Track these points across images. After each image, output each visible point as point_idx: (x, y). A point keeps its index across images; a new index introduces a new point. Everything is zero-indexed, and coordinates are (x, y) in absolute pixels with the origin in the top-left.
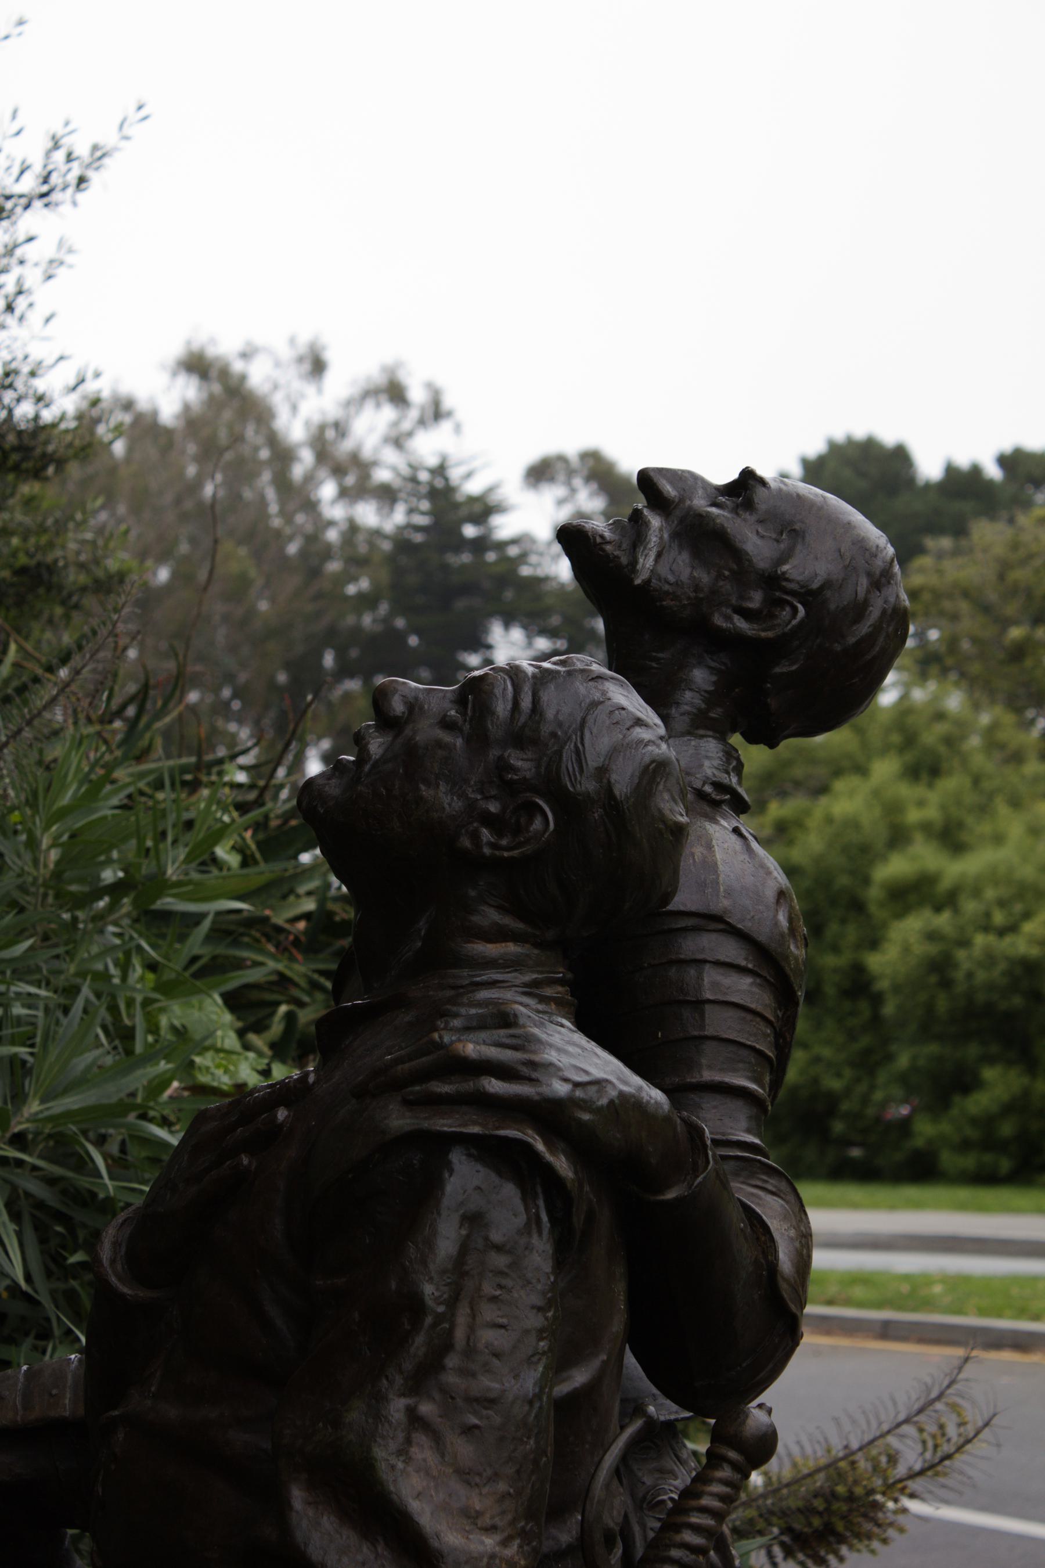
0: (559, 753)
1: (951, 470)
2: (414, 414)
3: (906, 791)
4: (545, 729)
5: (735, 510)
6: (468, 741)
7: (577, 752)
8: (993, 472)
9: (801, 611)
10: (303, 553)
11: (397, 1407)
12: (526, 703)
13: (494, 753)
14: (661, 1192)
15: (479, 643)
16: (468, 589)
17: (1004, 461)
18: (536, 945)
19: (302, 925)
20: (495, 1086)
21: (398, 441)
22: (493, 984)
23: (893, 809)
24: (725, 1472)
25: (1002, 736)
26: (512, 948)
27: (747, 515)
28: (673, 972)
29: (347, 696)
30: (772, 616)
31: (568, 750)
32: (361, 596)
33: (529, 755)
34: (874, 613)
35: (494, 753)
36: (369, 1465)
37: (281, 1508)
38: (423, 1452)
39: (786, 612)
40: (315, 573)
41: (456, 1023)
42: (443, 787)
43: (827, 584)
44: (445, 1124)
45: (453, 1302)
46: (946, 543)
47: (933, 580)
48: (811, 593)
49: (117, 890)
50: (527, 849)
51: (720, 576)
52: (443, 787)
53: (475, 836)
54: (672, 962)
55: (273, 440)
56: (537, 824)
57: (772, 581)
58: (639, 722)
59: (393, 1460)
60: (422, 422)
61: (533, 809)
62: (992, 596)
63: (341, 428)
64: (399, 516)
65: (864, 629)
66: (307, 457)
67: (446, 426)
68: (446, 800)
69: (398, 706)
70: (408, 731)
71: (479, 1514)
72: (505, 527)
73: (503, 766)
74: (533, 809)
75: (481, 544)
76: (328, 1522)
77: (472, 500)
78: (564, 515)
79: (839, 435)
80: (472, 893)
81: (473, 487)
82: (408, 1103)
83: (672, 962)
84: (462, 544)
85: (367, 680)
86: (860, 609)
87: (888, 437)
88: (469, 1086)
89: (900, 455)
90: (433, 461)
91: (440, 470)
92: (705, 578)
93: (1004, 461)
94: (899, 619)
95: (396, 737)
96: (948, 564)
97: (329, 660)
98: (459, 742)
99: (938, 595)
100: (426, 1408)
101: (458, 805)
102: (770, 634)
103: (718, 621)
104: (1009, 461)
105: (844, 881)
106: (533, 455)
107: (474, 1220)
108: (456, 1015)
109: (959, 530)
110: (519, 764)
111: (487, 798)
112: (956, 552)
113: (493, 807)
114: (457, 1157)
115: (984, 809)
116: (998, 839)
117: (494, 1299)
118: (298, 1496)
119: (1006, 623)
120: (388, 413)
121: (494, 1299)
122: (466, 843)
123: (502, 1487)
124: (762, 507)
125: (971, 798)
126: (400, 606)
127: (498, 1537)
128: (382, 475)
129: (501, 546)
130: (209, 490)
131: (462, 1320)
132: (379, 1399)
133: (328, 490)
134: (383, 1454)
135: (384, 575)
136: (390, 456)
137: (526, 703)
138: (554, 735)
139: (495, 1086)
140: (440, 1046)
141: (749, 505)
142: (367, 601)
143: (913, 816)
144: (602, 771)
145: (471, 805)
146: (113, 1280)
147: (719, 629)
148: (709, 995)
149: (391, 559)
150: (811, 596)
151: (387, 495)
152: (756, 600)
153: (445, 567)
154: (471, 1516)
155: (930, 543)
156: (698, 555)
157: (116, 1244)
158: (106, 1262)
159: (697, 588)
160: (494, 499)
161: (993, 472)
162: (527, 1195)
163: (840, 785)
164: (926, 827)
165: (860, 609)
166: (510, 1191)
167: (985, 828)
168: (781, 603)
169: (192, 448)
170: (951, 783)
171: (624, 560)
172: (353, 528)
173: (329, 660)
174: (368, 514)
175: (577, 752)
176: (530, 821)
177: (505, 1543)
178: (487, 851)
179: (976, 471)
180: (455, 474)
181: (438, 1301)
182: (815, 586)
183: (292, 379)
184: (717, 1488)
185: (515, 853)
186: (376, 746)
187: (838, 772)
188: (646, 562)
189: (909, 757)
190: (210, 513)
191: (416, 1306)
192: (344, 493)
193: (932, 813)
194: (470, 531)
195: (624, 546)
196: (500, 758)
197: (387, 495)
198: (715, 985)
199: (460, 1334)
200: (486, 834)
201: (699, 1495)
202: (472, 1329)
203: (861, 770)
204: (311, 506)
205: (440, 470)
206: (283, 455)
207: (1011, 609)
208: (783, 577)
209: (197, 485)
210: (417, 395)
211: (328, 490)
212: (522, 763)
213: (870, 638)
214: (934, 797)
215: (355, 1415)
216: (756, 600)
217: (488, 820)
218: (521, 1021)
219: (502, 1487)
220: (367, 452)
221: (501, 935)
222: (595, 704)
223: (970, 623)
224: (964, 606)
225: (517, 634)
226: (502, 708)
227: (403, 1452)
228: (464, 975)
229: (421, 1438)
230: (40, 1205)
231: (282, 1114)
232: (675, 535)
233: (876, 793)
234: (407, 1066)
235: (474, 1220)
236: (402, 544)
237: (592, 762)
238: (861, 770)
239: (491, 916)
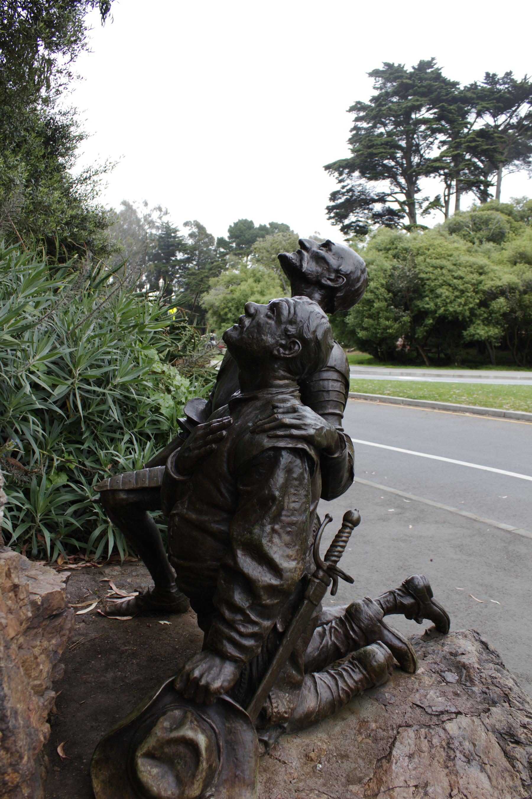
0: (303, 326)
1: (261, 226)
2: (162, 213)
3: (254, 285)
4: (298, 319)
5: (327, 251)
6: (276, 322)
7: (308, 326)
8: (268, 226)
9: (345, 280)
10: (142, 238)
11: (268, 528)
12: (292, 311)
13: (283, 326)
14: (333, 454)
15: (174, 255)
16: (173, 245)
17: (270, 224)
18: (292, 380)
19: (168, 328)
20: (295, 432)
21: (160, 218)
22: (282, 393)
23: (252, 288)
24: (348, 530)
25: (271, 275)
26: (286, 382)
27: (330, 253)
28: (321, 382)
29: (150, 265)
30: (337, 281)
31: (305, 325)
32: (153, 246)
33: (294, 327)
34: (362, 280)
35: (283, 326)
36: (261, 545)
37: (234, 557)
38: (276, 540)
39: (341, 280)
40: (144, 242)
41: (280, 410)
42: (269, 336)
43: (351, 272)
44: (281, 444)
45: (283, 497)
46: (261, 239)
47: (259, 246)
48: (347, 275)
49: (134, 327)
50: (294, 355)
51: (323, 269)
52: (269, 336)
53: (278, 351)
54: (321, 380)
55: (137, 217)
56: (297, 347)
57: (338, 271)
58: (323, 317)
59: (268, 544)
60: (164, 214)
61: (295, 343)
62: (269, 249)
63: (150, 215)
64: (160, 232)
65: (359, 284)
66: (143, 220)
67: (168, 215)
68: (270, 339)
69: (252, 311)
70: (257, 318)
71: (291, 556)
72: (179, 234)
73: (286, 330)
74: (295, 343)
75: (175, 237)
76: (248, 560)
77: (173, 229)
78: (190, 232)
79: (285, 223)
80: (276, 366)
81: (173, 227)
82: (268, 437)
83: (321, 380)
84: (172, 237)
85: (154, 262)
86: (358, 279)
87: (249, 220)
88: (287, 433)
89: (251, 222)
90: (166, 222)
91: (168, 223)
92: (319, 269)
93: (270, 224)
94: (367, 281)
95: (253, 320)
96: (262, 243)
97: (147, 258)
98: (273, 322)
99: (260, 249)
100: (277, 527)
101: (273, 341)
102: (337, 286)
103: (323, 281)
104: (271, 224)
105: (243, 301)
106: (185, 221)
107: (289, 471)
108: (280, 408)
109: (263, 237)
110: (291, 329)
111: (282, 339)
112: (263, 241)
113: (283, 342)
114: (284, 453)
115: (268, 288)
116: (271, 294)
117: (294, 494)
118: (239, 553)
119: (271, 254)
120: (158, 212)
121: (294, 494)
122: (276, 352)
123: (297, 547)
124: (334, 251)
125: (265, 286)
126: (160, 248)
127: (296, 562)
128: (157, 224)
129: (178, 237)
130: (125, 227)
131: (286, 501)
132: (263, 525)
133: (147, 227)
134: (264, 541)
135: (157, 243)
136: (159, 221)
137: (292, 311)
138: (301, 321)
139: (295, 432)
140: (277, 419)
141: (330, 250)
142: (154, 247)
143: (255, 289)
144: (314, 332)
145: (277, 341)
146: (172, 474)
147: (323, 284)
148: (330, 389)
149: (158, 240)
150: (347, 275)
151: (158, 228)
152: (333, 276)
153: (168, 241)
154: (289, 557)
155: (258, 239)
156: (317, 263)
157: (172, 463)
158: (170, 469)
159: (317, 273)
160: (177, 229)
161: (268, 226)
162: (303, 462)
163: (242, 283)
164: (258, 291)
165: (358, 279)
166: (298, 462)
167: (268, 292)
168: (340, 277)
169: (122, 219)
170: (262, 284)
171: (298, 264)
172: (151, 234)
173: (147, 258)
174: (154, 231)
175: (308, 326)
176: (294, 346)
177: (298, 563)
178: (282, 355)
179: (265, 226)
180: (170, 224)
181: (280, 496)
182: (348, 273)
183: (142, 206)
184: (346, 535)
185: (290, 356)
186: (247, 322)
187: (242, 281)
188: (305, 265)
189: (255, 278)
190: (124, 231)
191: (273, 498)
192: (150, 227)
193: (259, 289)
194: (173, 235)
195: (421, 287)
196: (285, 328)
197: (158, 228)
198: (332, 386)
199: (286, 504)
200: (281, 350)
201: (341, 537)
202: (289, 503)
203: (246, 281)
204: (144, 230)
205: (168, 223)
206: (139, 220)
207: (273, 252)
208: (341, 270)
209: (123, 225)
210: (164, 210)
211: (147, 227)
212: (292, 329)
213: (360, 287)
214: (259, 286)
215: (256, 530)
216: (333, 276)
217: (282, 346)
218: (300, 410)
219: (297, 547)
220: (154, 220)
221: (284, 378)
222: (311, 312)
223: (265, 254)
224: (264, 251)
225: (181, 254)
226: (285, 312)
227: (271, 541)
228: (274, 390)
229: (276, 536)
230: (119, 400)
231: (224, 433)
232: (311, 257)
233: (249, 285)
234: (268, 425)
235: (289, 471)
236: (161, 237)
237: (312, 329)
238: (246, 281)
239: (282, 373)
